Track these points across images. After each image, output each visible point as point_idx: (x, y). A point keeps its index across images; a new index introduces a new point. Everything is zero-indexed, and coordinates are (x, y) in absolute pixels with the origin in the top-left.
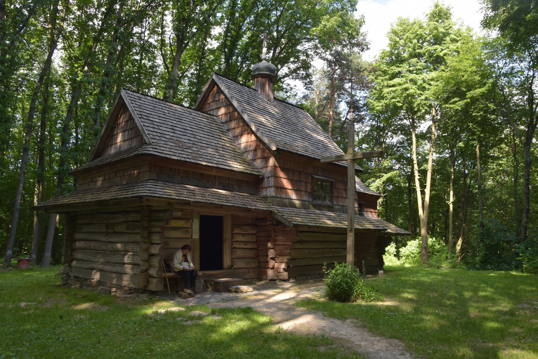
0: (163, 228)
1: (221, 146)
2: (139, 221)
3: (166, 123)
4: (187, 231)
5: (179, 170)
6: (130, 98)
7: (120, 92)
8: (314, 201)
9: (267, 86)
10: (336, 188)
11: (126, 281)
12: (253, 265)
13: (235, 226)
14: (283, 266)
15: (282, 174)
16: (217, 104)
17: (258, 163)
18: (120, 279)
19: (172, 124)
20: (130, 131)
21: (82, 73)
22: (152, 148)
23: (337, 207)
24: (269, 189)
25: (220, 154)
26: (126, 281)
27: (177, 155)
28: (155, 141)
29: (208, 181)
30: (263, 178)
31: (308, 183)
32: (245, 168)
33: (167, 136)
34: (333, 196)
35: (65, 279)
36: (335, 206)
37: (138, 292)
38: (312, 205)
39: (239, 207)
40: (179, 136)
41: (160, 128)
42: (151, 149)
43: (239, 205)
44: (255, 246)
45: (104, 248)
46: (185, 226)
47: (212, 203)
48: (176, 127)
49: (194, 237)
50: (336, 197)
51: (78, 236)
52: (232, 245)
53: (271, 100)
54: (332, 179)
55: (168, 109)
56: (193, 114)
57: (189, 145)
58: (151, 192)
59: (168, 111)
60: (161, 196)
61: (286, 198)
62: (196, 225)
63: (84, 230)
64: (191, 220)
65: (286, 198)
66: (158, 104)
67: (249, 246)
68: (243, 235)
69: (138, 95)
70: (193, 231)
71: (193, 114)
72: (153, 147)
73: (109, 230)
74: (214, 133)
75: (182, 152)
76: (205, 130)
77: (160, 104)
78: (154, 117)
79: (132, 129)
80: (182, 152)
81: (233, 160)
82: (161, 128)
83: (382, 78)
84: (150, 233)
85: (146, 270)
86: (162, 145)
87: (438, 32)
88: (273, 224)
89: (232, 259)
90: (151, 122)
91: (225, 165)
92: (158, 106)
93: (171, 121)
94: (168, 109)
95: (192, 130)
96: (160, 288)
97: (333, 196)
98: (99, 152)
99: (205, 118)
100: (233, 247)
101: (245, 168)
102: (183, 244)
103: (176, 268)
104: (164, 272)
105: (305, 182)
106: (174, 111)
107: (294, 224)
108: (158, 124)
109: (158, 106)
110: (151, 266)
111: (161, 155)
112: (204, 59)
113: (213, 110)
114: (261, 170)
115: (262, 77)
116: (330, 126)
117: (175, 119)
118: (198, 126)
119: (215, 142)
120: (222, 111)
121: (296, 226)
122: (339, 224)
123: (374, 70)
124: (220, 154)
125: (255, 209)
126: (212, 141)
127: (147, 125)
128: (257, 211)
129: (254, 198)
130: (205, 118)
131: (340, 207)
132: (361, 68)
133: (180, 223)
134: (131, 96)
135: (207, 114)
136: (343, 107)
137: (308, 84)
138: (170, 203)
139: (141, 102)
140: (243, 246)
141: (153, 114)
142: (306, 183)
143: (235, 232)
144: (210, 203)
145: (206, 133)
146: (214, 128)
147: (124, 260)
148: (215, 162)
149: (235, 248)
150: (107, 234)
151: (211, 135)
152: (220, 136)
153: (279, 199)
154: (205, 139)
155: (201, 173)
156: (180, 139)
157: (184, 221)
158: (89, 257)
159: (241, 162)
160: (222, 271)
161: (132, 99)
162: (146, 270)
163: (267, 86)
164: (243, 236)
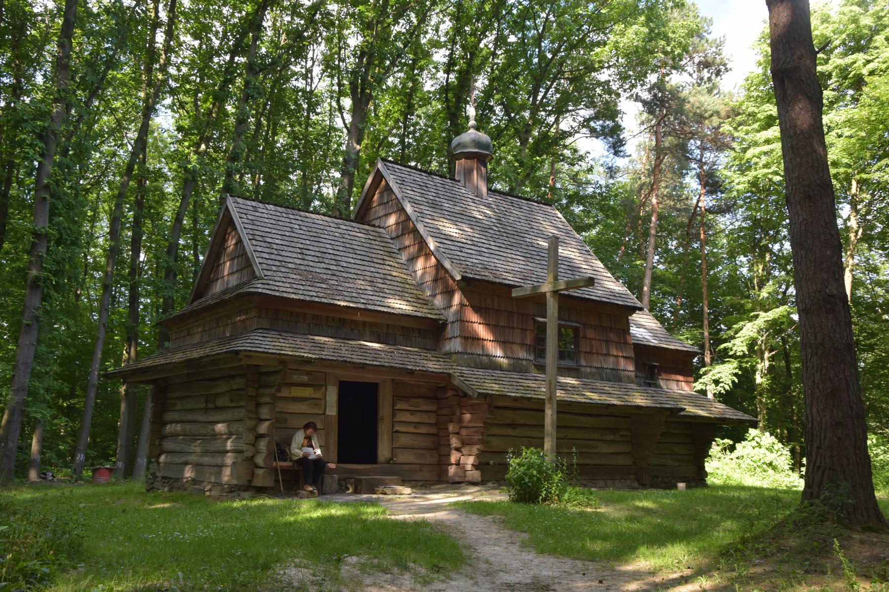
0: (275, 399)
1: (382, 276)
2: (243, 389)
3: (293, 244)
4: (316, 404)
5: (305, 314)
6: (239, 210)
7: (226, 202)
8: (539, 360)
9: (475, 172)
10: (585, 338)
11: (226, 476)
12: (429, 460)
13: (397, 397)
14: (470, 460)
15: (474, 317)
16: (385, 209)
17: (439, 301)
18: (219, 474)
19: (301, 246)
20: (240, 259)
21: (195, 157)
22: (262, 284)
23: (588, 370)
24: (453, 339)
25: (376, 289)
26: (226, 476)
27: (301, 292)
28: (269, 273)
29: (352, 330)
30: (445, 325)
31: (526, 330)
32: (415, 309)
33: (290, 265)
34: (580, 352)
35: (150, 481)
36: (583, 369)
37: (239, 490)
38: (536, 366)
39: (392, 367)
40: (311, 264)
41: (281, 253)
42: (260, 286)
43: (392, 365)
44: (434, 430)
45: (202, 431)
46: (313, 396)
47: (346, 361)
48: (308, 250)
49: (327, 413)
50: (585, 352)
51: (169, 416)
52: (393, 427)
53: (482, 195)
54: (577, 322)
55: (300, 223)
56: (342, 227)
57: (325, 277)
58: (252, 345)
59: (299, 225)
60: (266, 351)
61: (483, 355)
62: (332, 396)
63: (178, 407)
64: (324, 388)
65: (483, 355)
66: (285, 215)
67: (423, 430)
68: (412, 412)
69: (254, 204)
70: (327, 404)
71: (342, 227)
72: (265, 282)
73: (210, 405)
74: (373, 256)
75: (310, 288)
76: (358, 252)
77: (288, 216)
78: (274, 236)
79: (242, 255)
80: (310, 288)
81: (397, 298)
82: (283, 253)
83: (747, 128)
84: (258, 405)
85: (252, 457)
86: (279, 279)
87: (858, 27)
88: (458, 395)
89: (393, 449)
90: (268, 245)
91: (379, 305)
92: (283, 219)
93: (301, 241)
94: (300, 223)
95: (335, 252)
96: (269, 482)
97: (580, 352)
98: (200, 292)
99: (363, 231)
100: (394, 430)
101: (415, 309)
102: (305, 422)
103: (295, 455)
104: (275, 460)
105: (522, 329)
106: (310, 225)
107: (479, 393)
108: (278, 247)
109: (283, 219)
110: (258, 452)
111: (273, 293)
112: (412, 115)
113: (380, 218)
114: (443, 311)
115: (466, 158)
116: (652, 225)
117: (309, 238)
118: (348, 246)
119: (373, 269)
120: (392, 220)
121: (485, 396)
122: (576, 396)
123: (734, 112)
124: (376, 289)
125: (419, 370)
126: (368, 268)
127: (259, 249)
128: (426, 374)
129: (428, 355)
130: (363, 231)
131: (594, 370)
132: (706, 111)
133: (308, 392)
134: (241, 206)
135: (369, 225)
136: (692, 183)
137: (617, 147)
138: (283, 360)
139: (257, 214)
140: (411, 429)
141: (274, 231)
142: (524, 330)
143: (398, 407)
144: (342, 361)
145: (359, 257)
146: (376, 247)
147: (226, 446)
148: (362, 301)
149: (397, 432)
150: (206, 410)
151: (368, 259)
152: (383, 259)
153: (471, 356)
154: (355, 266)
155: (340, 319)
156: (311, 269)
157: (312, 389)
158: (183, 446)
159: (410, 299)
160: (374, 466)
161: (242, 211)
162: (252, 457)
163: (475, 172)
164: (412, 414)
